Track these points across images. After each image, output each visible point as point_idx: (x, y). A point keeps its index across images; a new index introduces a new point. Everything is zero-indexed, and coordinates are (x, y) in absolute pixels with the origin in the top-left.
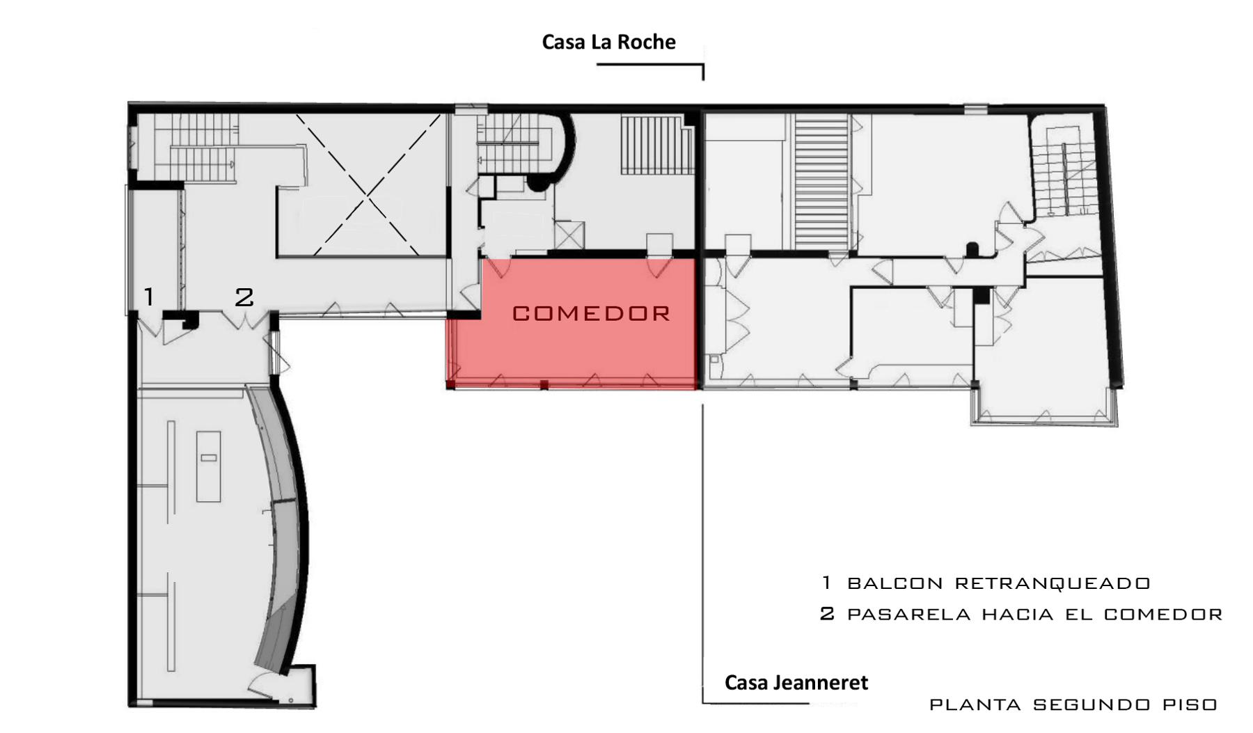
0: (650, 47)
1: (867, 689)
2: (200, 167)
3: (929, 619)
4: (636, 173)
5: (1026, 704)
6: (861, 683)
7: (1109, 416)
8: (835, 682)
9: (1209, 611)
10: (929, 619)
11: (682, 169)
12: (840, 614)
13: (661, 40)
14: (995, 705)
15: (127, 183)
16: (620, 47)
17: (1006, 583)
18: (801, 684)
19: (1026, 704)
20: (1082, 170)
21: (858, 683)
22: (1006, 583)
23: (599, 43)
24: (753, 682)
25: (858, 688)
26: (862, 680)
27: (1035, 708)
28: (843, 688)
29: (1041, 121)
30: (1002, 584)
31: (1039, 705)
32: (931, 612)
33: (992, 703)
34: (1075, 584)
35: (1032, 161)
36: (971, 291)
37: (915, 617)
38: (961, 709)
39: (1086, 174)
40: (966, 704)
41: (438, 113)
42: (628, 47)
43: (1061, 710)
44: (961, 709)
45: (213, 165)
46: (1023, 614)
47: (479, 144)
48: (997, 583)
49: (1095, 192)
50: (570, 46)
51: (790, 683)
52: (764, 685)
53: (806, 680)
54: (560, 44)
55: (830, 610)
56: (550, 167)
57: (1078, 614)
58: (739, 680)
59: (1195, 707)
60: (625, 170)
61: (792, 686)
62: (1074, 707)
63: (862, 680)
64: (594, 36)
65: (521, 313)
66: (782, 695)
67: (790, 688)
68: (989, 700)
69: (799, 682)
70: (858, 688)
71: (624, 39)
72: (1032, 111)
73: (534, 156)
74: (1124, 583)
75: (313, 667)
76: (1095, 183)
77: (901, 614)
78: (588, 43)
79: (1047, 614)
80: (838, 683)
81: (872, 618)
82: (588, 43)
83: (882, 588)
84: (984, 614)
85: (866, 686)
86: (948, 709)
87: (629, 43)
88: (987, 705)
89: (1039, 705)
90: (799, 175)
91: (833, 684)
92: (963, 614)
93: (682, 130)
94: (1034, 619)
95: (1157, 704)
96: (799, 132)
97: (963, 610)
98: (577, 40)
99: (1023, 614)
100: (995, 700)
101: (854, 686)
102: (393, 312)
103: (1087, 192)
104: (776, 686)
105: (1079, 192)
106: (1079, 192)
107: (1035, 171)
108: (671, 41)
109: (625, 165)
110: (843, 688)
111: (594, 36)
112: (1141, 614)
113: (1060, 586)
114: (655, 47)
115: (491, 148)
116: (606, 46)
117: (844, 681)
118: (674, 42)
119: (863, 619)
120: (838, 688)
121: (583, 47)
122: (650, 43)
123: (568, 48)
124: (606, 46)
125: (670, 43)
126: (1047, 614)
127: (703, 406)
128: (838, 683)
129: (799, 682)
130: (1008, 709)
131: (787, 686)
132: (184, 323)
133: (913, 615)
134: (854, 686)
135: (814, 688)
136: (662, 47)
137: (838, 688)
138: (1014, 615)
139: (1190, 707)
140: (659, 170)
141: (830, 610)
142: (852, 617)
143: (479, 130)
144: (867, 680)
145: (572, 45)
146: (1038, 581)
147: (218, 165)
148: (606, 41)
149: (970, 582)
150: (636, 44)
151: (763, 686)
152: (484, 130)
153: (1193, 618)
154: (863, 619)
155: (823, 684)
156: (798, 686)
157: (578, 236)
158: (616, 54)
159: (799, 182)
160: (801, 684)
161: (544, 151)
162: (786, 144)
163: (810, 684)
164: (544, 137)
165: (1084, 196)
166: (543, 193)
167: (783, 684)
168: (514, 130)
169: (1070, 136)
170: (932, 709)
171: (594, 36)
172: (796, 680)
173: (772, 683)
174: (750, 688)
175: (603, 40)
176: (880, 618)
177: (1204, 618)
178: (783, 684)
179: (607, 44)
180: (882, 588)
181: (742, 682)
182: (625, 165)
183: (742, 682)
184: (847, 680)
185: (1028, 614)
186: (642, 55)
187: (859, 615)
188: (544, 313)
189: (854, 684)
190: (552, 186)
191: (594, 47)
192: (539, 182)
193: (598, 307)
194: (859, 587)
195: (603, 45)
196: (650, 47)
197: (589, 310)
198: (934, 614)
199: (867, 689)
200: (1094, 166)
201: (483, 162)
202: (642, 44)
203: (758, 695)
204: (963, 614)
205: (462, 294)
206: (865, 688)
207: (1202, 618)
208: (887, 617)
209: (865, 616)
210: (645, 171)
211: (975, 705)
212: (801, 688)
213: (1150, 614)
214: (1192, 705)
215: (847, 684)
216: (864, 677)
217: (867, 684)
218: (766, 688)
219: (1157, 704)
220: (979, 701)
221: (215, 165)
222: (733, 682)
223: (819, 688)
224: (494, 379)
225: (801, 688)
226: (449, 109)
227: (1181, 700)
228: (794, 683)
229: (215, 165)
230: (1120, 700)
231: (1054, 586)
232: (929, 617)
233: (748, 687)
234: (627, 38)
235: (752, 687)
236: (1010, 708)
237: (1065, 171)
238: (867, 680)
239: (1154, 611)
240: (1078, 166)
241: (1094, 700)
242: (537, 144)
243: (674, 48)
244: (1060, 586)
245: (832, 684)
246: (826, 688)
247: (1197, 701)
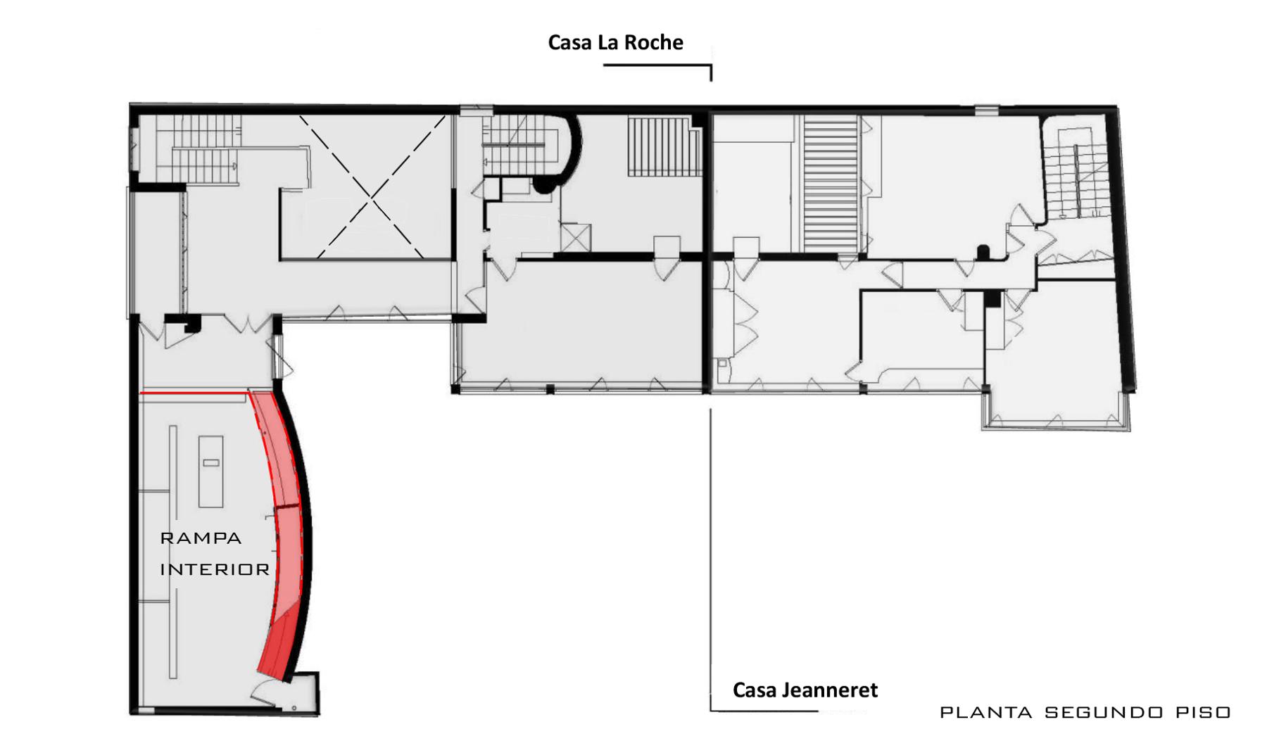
0: (658, 48)
1: (877, 696)
4: (643, 175)
5: (1038, 711)
6: (871, 690)
7: (1121, 421)
8: (844, 689)
13: (669, 40)
14: (1006, 712)
15: (128, 185)
16: (627, 48)
18: (810, 692)
19: (1038, 711)
21: (868, 691)
23: (605, 44)
24: (762, 689)
25: (867, 696)
26: (871, 687)
27: (1047, 716)
28: (853, 695)
31: (1051, 712)
32: (1066, 710)
33: (1004, 710)
34: (1101, 713)
35: (1043, 162)
38: (972, 717)
39: (1099, 176)
40: (977, 712)
41: (443, 114)
42: (635, 48)
43: (1072, 717)
44: (972, 717)
47: (484, 145)
49: (1107, 194)
50: (576, 46)
51: (799, 691)
52: (773, 692)
53: (815, 687)
54: (566, 45)
56: (556, 169)
58: (747, 688)
60: (632, 172)
61: (801, 694)
62: (1086, 715)
63: (871, 687)
64: (601, 37)
66: (791, 702)
67: (799, 696)
68: (1000, 708)
69: (808, 689)
70: (867, 696)
71: (631, 39)
73: (540, 158)
75: (316, 675)
76: (1107, 185)
78: (595, 44)
80: (847, 691)
82: (595, 44)
85: (876, 694)
86: (958, 717)
87: (636, 43)
88: (998, 712)
89: (1051, 712)
90: (808, 176)
91: (842, 692)
93: (689, 132)
95: (1169, 712)
96: (808, 133)
97: (977, 708)
98: (583, 40)
100: (1006, 708)
101: (864, 694)
102: (397, 315)
103: (1099, 194)
104: (784, 693)
105: (1091, 195)
106: (1091, 195)
107: (1047, 173)
108: (678, 42)
109: (632, 167)
110: (853, 695)
111: (601, 37)
114: (663, 48)
115: (496, 150)
116: (613, 46)
117: (853, 689)
118: (682, 43)
120: (847, 696)
122: (657, 44)
124: (613, 46)
125: (677, 44)
128: (847, 691)
129: (808, 689)
130: (1019, 717)
131: (796, 694)
132: (186, 327)
134: (864, 694)
135: (823, 695)
137: (847, 696)
139: (1203, 715)
140: (667, 172)
142: (944, 715)
143: (485, 132)
144: (877, 687)
145: (578, 45)
148: (613, 42)
150: (644, 44)
152: (489, 132)
155: (832, 691)
156: (807, 694)
157: (585, 238)
158: (623, 54)
159: (808, 184)
160: (810, 692)
161: (550, 153)
162: (795, 146)
163: (819, 691)
164: (550, 139)
166: (550, 195)
167: (792, 691)
168: (520, 131)
170: (942, 717)
171: (601, 37)
172: (804, 688)
173: (781, 690)
174: (759, 696)
175: (610, 40)
177: (1106, 717)
178: (792, 691)
179: (614, 45)
181: (750, 689)
182: (632, 167)
183: (750, 689)
184: (857, 687)
186: (649, 56)
187: (225, 538)
188: (245, 570)
189: (863, 691)
190: (558, 188)
191: (601, 47)
192: (545, 184)
195: (610, 45)
196: (658, 48)
197: (204, 567)
199: (877, 696)
200: (1106, 168)
201: (488, 164)
202: (649, 44)
203: (766, 703)
205: (468, 297)
206: (875, 695)
209: (230, 540)
211: (986, 713)
212: (810, 695)
214: (1206, 712)
215: (857, 691)
216: (874, 684)
217: (877, 692)
218: (774, 695)
219: (1169, 712)
220: (990, 709)
222: (741, 690)
223: (829, 695)
224: (499, 384)
225: (810, 695)
226: (454, 110)
227: (1194, 708)
228: (803, 691)
230: (1132, 708)
233: (756, 695)
234: (634, 38)
235: (761, 694)
236: (1021, 716)
237: (1077, 173)
238: (877, 687)
240: (1090, 168)
241: (1106, 708)
242: (543, 145)
243: (681, 48)
245: (841, 691)
246: (835, 696)
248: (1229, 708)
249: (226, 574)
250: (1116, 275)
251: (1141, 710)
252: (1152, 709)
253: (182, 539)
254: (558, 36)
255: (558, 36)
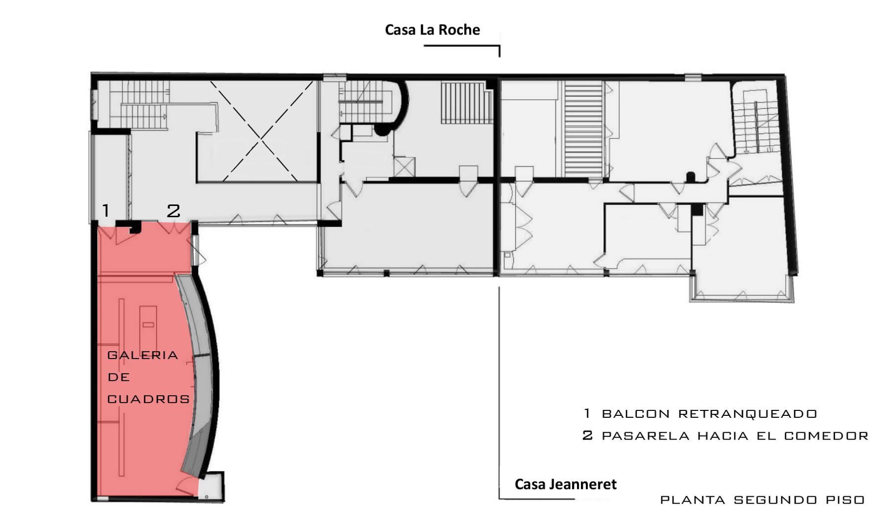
0: (462, 34)
1: (616, 488)
2: (142, 118)
3: (660, 439)
4: (452, 123)
5: (729, 499)
6: (612, 484)
8: (593, 484)
9: (859, 434)
10: (660, 439)
11: (484, 120)
12: (597, 435)
13: (470, 28)
14: (706, 500)
15: (90, 130)
16: (441, 34)
17: (714, 413)
18: (569, 486)
19: (729, 499)
20: (768, 121)
21: (609, 485)
22: (714, 413)
23: (425, 31)
24: (535, 484)
25: (609, 488)
26: (612, 482)
27: (735, 503)
28: (599, 488)
29: (739, 86)
30: (712, 414)
31: (738, 500)
32: (662, 434)
33: (705, 498)
34: (763, 414)
35: (733, 114)
36: (689, 206)
37: (650, 438)
38: (682, 503)
39: (772, 124)
40: (686, 500)
42: (446, 34)
43: (753, 503)
44: (682, 503)
45: (151, 117)
46: (727, 436)
47: (340, 102)
48: (708, 414)
49: (778, 136)
50: (405, 33)
51: (561, 485)
52: (543, 486)
53: (573, 482)
54: (398, 31)
55: (590, 433)
56: (391, 119)
57: (765, 436)
58: (525, 483)
59: (849, 502)
60: (444, 120)
61: (563, 487)
63: (612, 482)
64: (422, 26)
65: (789, 436)
66: (555, 493)
67: (561, 488)
68: (703, 497)
69: (567, 484)
70: (609, 488)
71: (443, 27)
72: (733, 79)
73: (379, 111)
74: (798, 414)
75: (222, 473)
76: (778, 130)
77: (640, 436)
78: (418, 31)
79: (743, 436)
80: (595, 485)
81: (619, 438)
82: (418, 31)
83: (627, 417)
84: (699, 436)
85: (615, 487)
86: (673, 503)
87: (447, 30)
88: (701, 500)
89: (738, 500)
90: (567, 124)
91: (592, 485)
92: (684, 436)
93: (484, 92)
94: (735, 439)
95: (822, 500)
96: (568, 94)
97: (684, 433)
98: (410, 28)
99: (727, 436)
100: (707, 497)
101: (607, 487)
102: (279, 221)
103: (772, 136)
104: (551, 487)
105: (766, 137)
106: (766, 137)
107: (735, 121)
108: (476, 29)
109: (444, 117)
110: (599, 488)
111: (422, 26)
112: (811, 435)
113: (753, 416)
114: (465, 34)
115: (349, 105)
116: (431, 32)
117: (599, 483)
118: (479, 30)
119: (613, 439)
120: (595, 488)
121: (414, 34)
122: (462, 31)
123: (403, 34)
124: (431, 32)
125: (476, 31)
126: (743, 436)
127: (499, 288)
128: (595, 485)
129: (567, 484)
130: (716, 503)
131: (559, 487)
132: (130, 229)
133: (649, 436)
134: (607, 487)
135: (578, 488)
136: (470, 34)
137: (595, 488)
138: (721, 436)
140: (468, 121)
141: (590, 433)
142: (605, 438)
143: (340, 92)
144: (616, 482)
145: (406, 32)
146: (737, 412)
147: (155, 117)
148: (431, 29)
149: (689, 413)
150: (452, 31)
151: (542, 487)
152: (344, 92)
153: (847, 439)
154: (613, 439)
155: (584, 485)
156: (567, 487)
157: (411, 167)
158: (437, 38)
159: (567, 129)
160: (569, 486)
161: (387, 107)
162: (559, 102)
163: (576, 485)
164: (387, 97)
165: (770, 139)
166: (386, 137)
167: (556, 485)
168: (365, 92)
169: (760, 97)
170: (662, 503)
171: (422, 26)
172: (565, 483)
173: (548, 485)
174: (533, 488)
175: (428, 28)
176: (625, 439)
177: (855, 439)
178: (556, 485)
179: (431, 31)
180: (627, 417)
181: (527, 484)
182: (444, 117)
183: (527, 484)
184: (602, 482)
185: (730, 436)
186: (456, 39)
187: (610, 436)
188: (172, 399)
189: (606, 485)
190: (392, 132)
191: (422, 33)
192: (383, 129)
193: (666, 432)
194: (610, 417)
195: (428, 32)
196: (462, 34)
198: (663, 436)
199: (616, 488)
200: (777, 118)
201: (343, 115)
202: (456, 31)
203: (538, 493)
204: (684, 436)
205: (328, 209)
206: (614, 488)
207: (854, 438)
208: (630, 438)
209: (614, 437)
210: (458, 122)
211: (692, 500)
212: (569, 488)
213: (817, 436)
214: (847, 500)
215: (602, 485)
216: (614, 480)
217: (616, 485)
218: (544, 488)
219: (822, 500)
220: (695, 497)
221: (153, 117)
222: (521, 484)
223: (582, 488)
224: (351, 269)
225: (569, 488)
226: (319, 77)
227: (839, 497)
228: (564, 485)
229: (153, 117)
231: (749, 416)
232: (660, 438)
233: (531, 488)
234: (446, 27)
235: (534, 487)
236: (718, 503)
237: (757, 121)
238: (616, 482)
239: (820, 433)
240: (765, 118)
241: (777, 497)
242: (381, 102)
243: (478, 34)
244: (753, 416)
245: (591, 485)
246: (587, 488)
247: (850, 497)
248: (863, 497)
249: (655, 439)
250: (784, 193)
251: (801, 498)
252: (804, 438)
253: (135, 398)
254: (392, 26)
255: (392, 26)
